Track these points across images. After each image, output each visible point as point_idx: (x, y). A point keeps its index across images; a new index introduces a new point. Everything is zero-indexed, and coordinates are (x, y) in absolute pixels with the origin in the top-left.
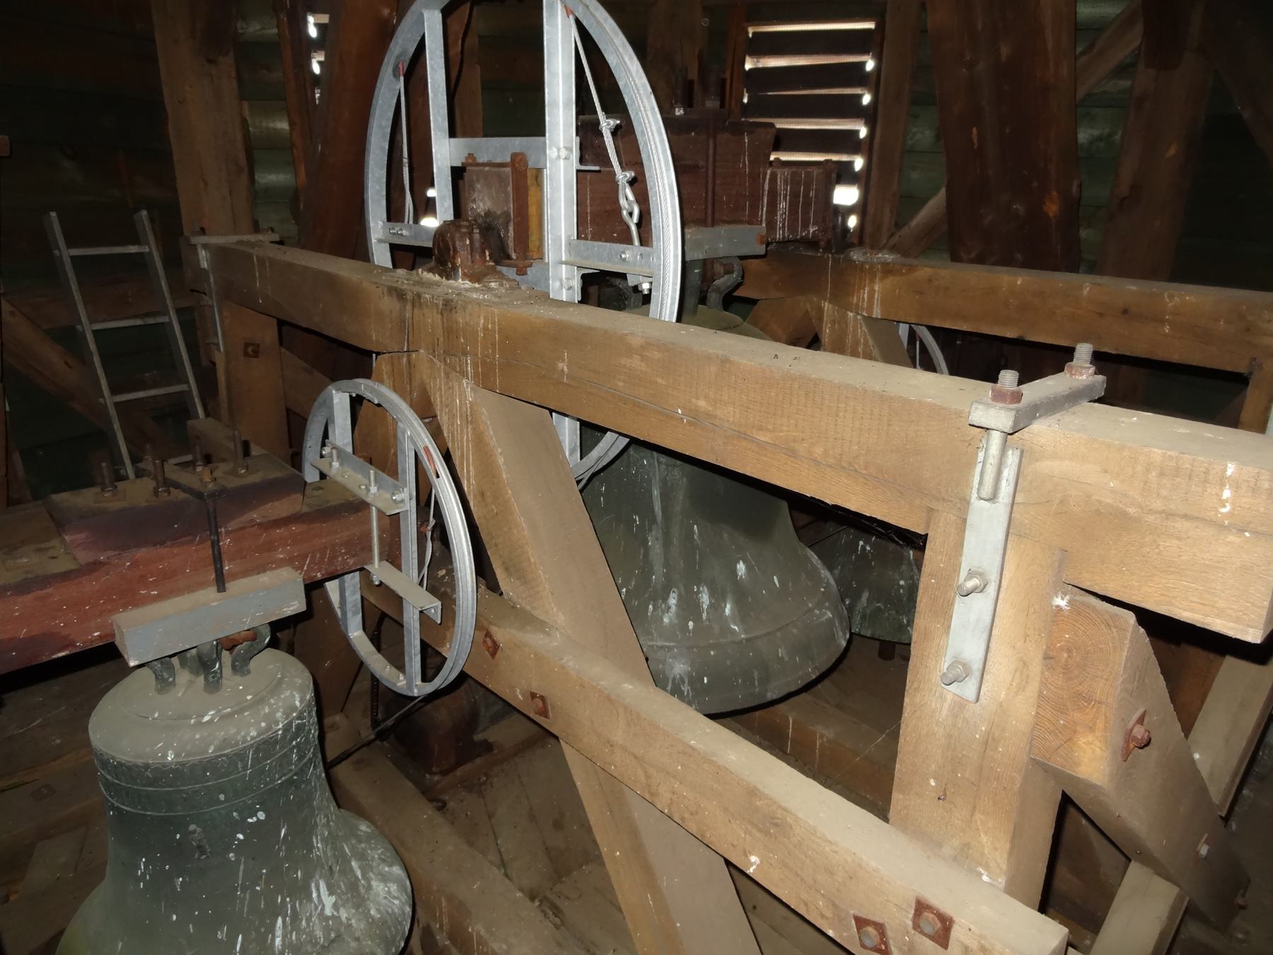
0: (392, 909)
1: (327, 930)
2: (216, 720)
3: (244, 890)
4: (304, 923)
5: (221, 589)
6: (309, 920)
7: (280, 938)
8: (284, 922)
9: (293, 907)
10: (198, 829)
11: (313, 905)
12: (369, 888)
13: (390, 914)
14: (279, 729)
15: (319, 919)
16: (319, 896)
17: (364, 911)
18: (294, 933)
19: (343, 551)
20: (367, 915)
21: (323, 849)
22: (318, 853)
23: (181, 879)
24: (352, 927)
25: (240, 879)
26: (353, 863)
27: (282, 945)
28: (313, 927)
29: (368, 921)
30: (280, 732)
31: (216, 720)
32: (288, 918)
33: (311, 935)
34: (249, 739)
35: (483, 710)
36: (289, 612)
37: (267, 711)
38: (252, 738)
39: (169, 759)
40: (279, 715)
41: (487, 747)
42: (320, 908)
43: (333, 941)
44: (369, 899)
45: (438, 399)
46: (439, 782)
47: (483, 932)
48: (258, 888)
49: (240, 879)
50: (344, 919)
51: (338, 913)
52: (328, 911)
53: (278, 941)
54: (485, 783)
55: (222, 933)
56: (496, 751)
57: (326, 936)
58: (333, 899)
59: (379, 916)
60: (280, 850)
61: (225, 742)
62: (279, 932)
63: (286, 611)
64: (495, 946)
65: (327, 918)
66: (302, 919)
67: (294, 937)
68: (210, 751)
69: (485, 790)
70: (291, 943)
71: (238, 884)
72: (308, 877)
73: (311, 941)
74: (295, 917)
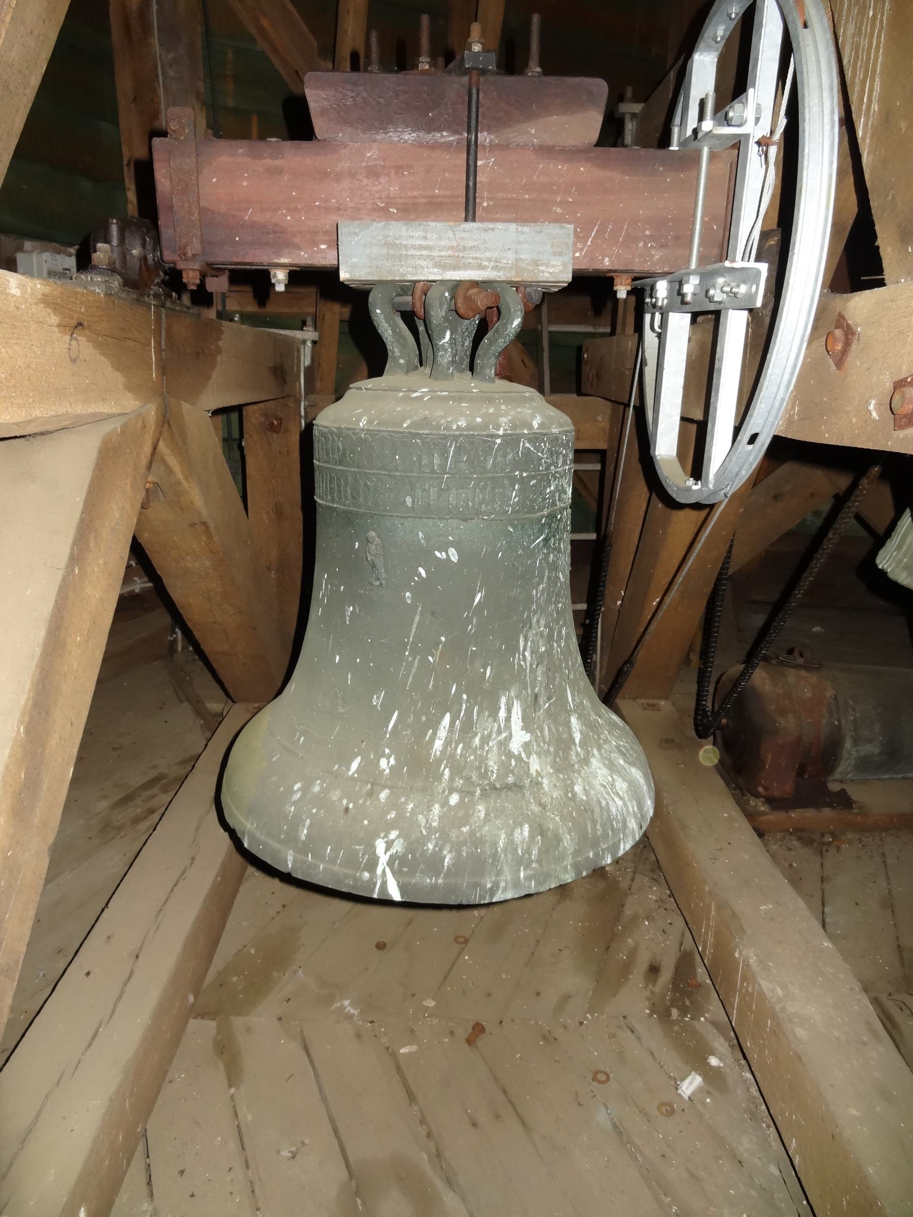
0: (607, 803)
1: (505, 769)
2: (425, 399)
3: (414, 653)
4: (477, 740)
5: (470, 217)
6: (485, 740)
7: (442, 742)
8: (452, 724)
9: (469, 712)
10: (377, 539)
11: (496, 725)
12: (585, 761)
13: (601, 808)
14: (499, 436)
15: (500, 749)
16: (508, 719)
17: (564, 780)
18: (461, 746)
19: (647, 233)
20: (568, 787)
21: (531, 665)
22: (522, 663)
23: (351, 609)
24: (542, 788)
25: (412, 634)
26: (574, 720)
27: (441, 752)
28: (487, 752)
29: (566, 794)
30: (499, 441)
31: (425, 399)
32: (458, 721)
33: (483, 760)
34: (454, 428)
35: (848, 744)
36: (547, 274)
37: (490, 412)
38: (459, 428)
39: (361, 425)
40: (503, 420)
41: (844, 801)
42: (504, 735)
43: (508, 787)
44: (579, 772)
45: (843, 22)
46: (763, 813)
47: (753, 961)
48: (430, 658)
49: (412, 634)
50: (533, 771)
51: (528, 757)
52: (515, 746)
53: (438, 745)
54: (830, 843)
55: (378, 698)
56: (856, 811)
57: (502, 776)
58: (527, 737)
59: (585, 798)
60: (469, 621)
61: (425, 422)
62: (442, 733)
63: (543, 272)
64: (765, 985)
65: (510, 755)
66: (476, 735)
67: (459, 751)
68: (405, 425)
69: (827, 851)
70: (453, 756)
71: (409, 640)
72: (500, 684)
73: (479, 768)
74: (468, 727)
